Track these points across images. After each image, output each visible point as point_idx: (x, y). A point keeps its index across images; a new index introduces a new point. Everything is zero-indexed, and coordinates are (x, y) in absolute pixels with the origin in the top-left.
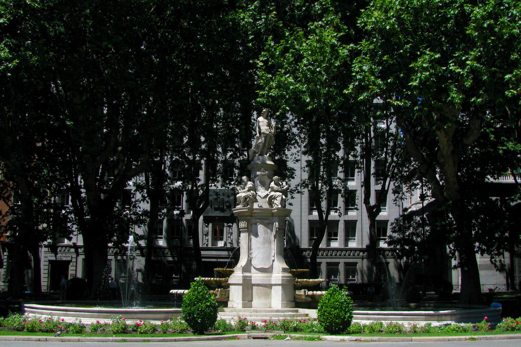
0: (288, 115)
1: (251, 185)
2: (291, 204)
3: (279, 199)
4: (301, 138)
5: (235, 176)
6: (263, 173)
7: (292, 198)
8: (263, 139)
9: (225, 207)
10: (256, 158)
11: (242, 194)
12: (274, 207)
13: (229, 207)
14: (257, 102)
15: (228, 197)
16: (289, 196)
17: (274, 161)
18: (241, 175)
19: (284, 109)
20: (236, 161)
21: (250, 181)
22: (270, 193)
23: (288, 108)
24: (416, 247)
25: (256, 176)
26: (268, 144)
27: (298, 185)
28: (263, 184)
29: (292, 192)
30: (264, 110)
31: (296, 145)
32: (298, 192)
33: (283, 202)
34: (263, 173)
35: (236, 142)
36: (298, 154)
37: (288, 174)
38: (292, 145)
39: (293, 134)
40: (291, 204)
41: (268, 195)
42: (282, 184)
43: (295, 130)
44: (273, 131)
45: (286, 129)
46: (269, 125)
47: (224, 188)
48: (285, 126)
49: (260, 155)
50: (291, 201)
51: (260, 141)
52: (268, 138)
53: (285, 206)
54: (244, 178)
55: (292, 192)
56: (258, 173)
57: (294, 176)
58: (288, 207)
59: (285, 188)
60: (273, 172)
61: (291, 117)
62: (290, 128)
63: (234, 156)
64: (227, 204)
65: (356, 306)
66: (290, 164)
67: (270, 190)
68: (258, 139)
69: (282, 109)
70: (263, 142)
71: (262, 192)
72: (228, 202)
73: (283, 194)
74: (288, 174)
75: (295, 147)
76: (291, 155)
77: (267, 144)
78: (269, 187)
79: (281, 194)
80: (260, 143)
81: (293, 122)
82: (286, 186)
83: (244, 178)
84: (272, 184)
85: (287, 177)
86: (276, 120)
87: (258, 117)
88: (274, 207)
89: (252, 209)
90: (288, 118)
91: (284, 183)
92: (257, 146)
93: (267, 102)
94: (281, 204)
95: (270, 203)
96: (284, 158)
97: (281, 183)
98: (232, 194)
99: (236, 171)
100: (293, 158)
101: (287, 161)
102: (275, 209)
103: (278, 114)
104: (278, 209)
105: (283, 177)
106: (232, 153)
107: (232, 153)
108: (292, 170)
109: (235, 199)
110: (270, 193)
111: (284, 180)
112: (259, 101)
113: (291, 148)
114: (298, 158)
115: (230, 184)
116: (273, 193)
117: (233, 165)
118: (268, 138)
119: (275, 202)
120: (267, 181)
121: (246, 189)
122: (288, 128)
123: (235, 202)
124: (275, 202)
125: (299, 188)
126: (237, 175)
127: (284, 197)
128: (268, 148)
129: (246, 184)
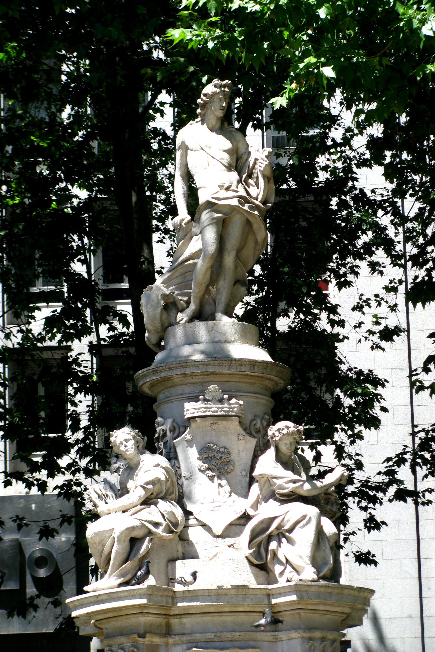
0: (334, 104)
1: (161, 475)
2: (365, 558)
3: (305, 537)
4: (404, 220)
5: (75, 428)
6: (215, 408)
7: (372, 524)
8: (211, 235)
9: (31, 590)
10: (179, 333)
11: (113, 519)
12: (282, 582)
13: (52, 587)
14: (172, 49)
15: (47, 533)
16: (356, 516)
17: (270, 340)
18: (105, 419)
19: (312, 77)
20: (80, 347)
21: (153, 450)
22: (255, 506)
23: (328, 72)
24: (240, 86)
25: (182, 425)
26: (238, 257)
27: (400, 460)
28: (217, 462)
29: (368, 494)
30: (209, 89)
31: (380, 255)
32: (402, 495)
33: (327, 551)
34: (215, 408)
35: (73, 254)
36: (391, 298)
37: (347, 402)
38: (359, 256)
39: (361, 198)
40: (365, 558)
41: (246, 518)
42: (318, 458)
43: (372, 180)
44: (258, 191)
45: (323, 176)
46: (238, 162)
47: (18, 488)
48: (322, 160)
49: (200, 316)
50: (364, 541)
51: (195, 245)
52: (235, 231)
53: (335, 574)
54: (124, 438)
55: (368, 494)
56: (191, 409)
57: (377, 411)
58: (352, 574)
59: (330, 479)
60: (264, 403)
61: (347, 118)
62: (348, 170)
63: (66, 324)
64: (42, 573)
65: (380, 266)
66: (354, 354)
67: (255, 489)
68: (183, 234)
69: (297, 78)
70: (212, 247)
71: (213, 501)
72: (41, 562)
73: (323, 512)
74: (347, 402)
75: (374, 266)
76: (358, 308)
77: (229, 260)
78: (252, 480)
79: (312, 511)
80: (195, 255)
81: (360, 142)
82: (339, 472)
83: (124, 438)
84: (267, 464)
85: (342, 419)
86: (272, 133)
87: (179, 124)
88: (282, 582)
89: (165, 597)
90: (333, 120)
91: (328, 451)
92: (182, 271)
93: (222, 44)
94: (315, 562)
95: (262, 564)
96: (323, 324)
97: (309, 455)
98: (65, 519)
99: (83, 404)
100: (368, 325)
101: (336, 338)
102: (282, 592)
103: (280, 102)
104: (299, 589)
105: (321, 422)
106: (58, 307)
107: (58, 307)
108: (366, 384)
109: (81, 548)
110: (255, 506)
111: (326, 435)
112: (183, 44)
113: (354, 271)
114: (392, 321)
115: (54, 470)
116: (271, 509)
117: (65, 368)
118: (235, 231)
119: (284, 550)
120: (241, 447)
121: (136, 494)
122: (334, 172)
123: (83, 566)
124: (284, 550)
125: (404, 473)
126: (84, 422)
127: (329, 527)
128: (237, 282)
129: (131, 469)
